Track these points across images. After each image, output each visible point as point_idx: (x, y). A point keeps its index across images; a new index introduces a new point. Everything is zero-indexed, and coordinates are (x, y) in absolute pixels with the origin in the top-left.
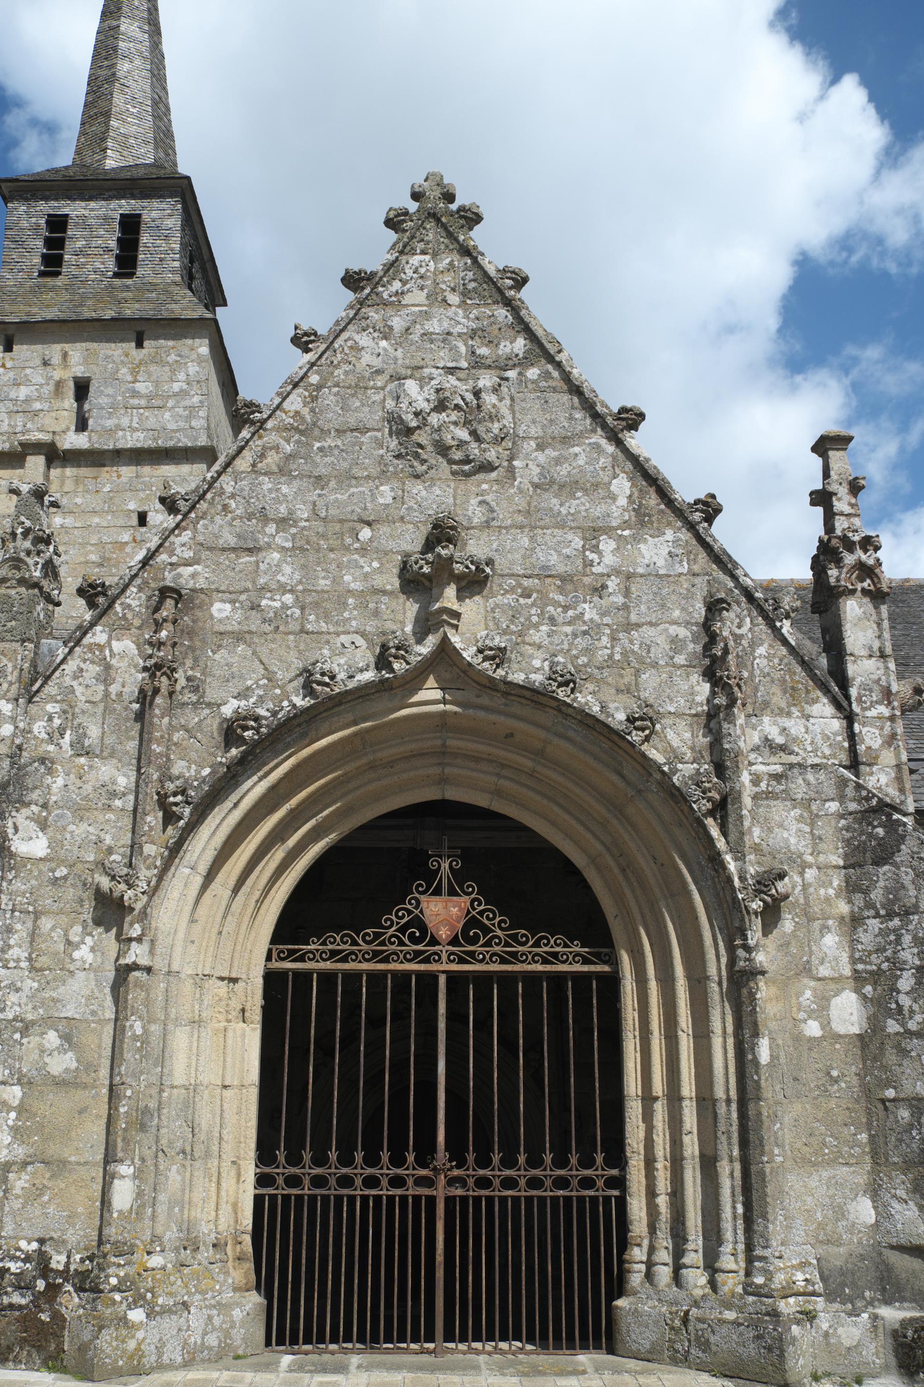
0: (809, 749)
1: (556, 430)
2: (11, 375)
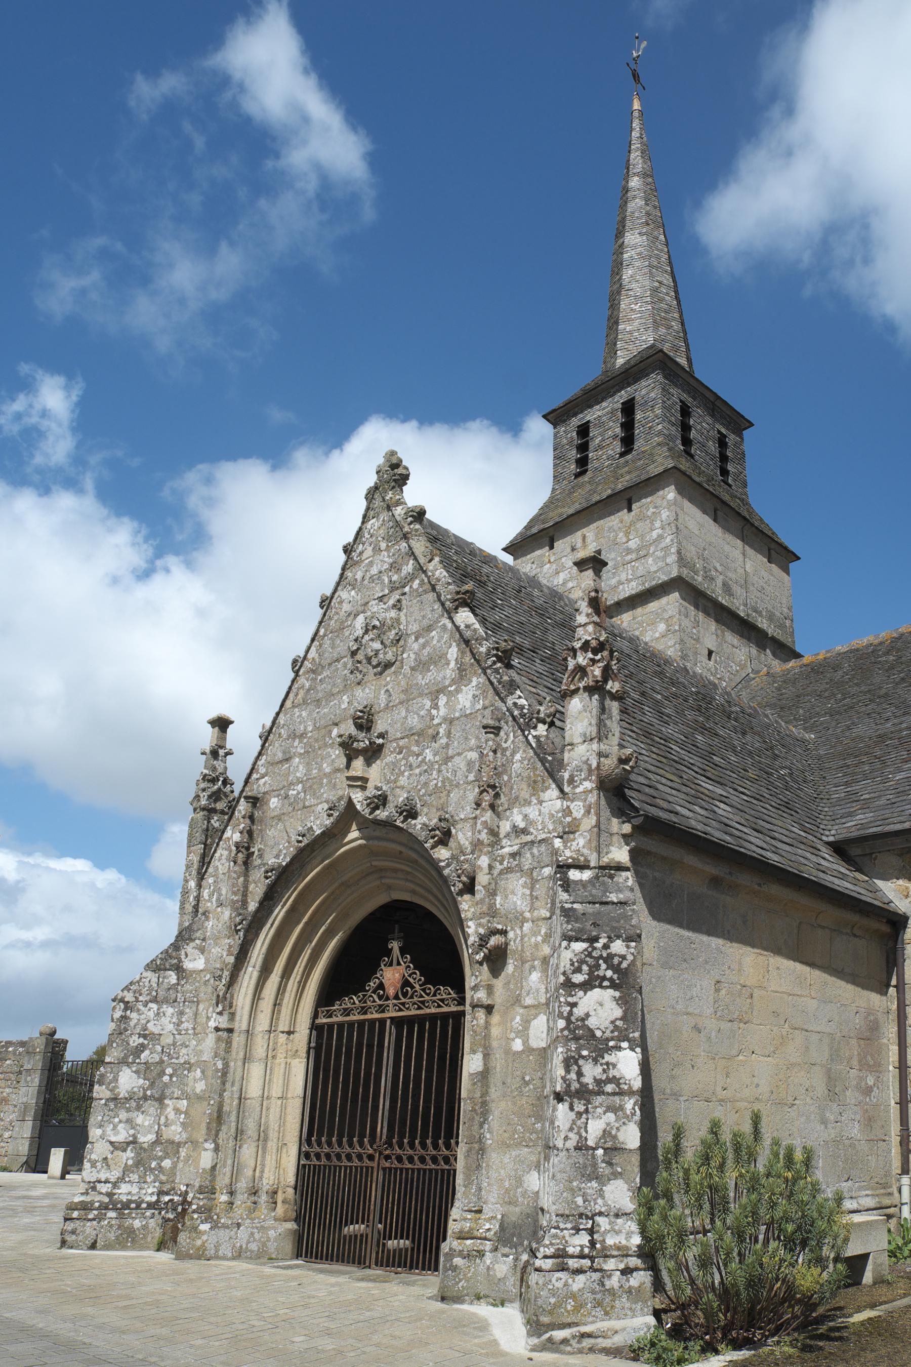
1: (426, 623)
2: (554, 566)
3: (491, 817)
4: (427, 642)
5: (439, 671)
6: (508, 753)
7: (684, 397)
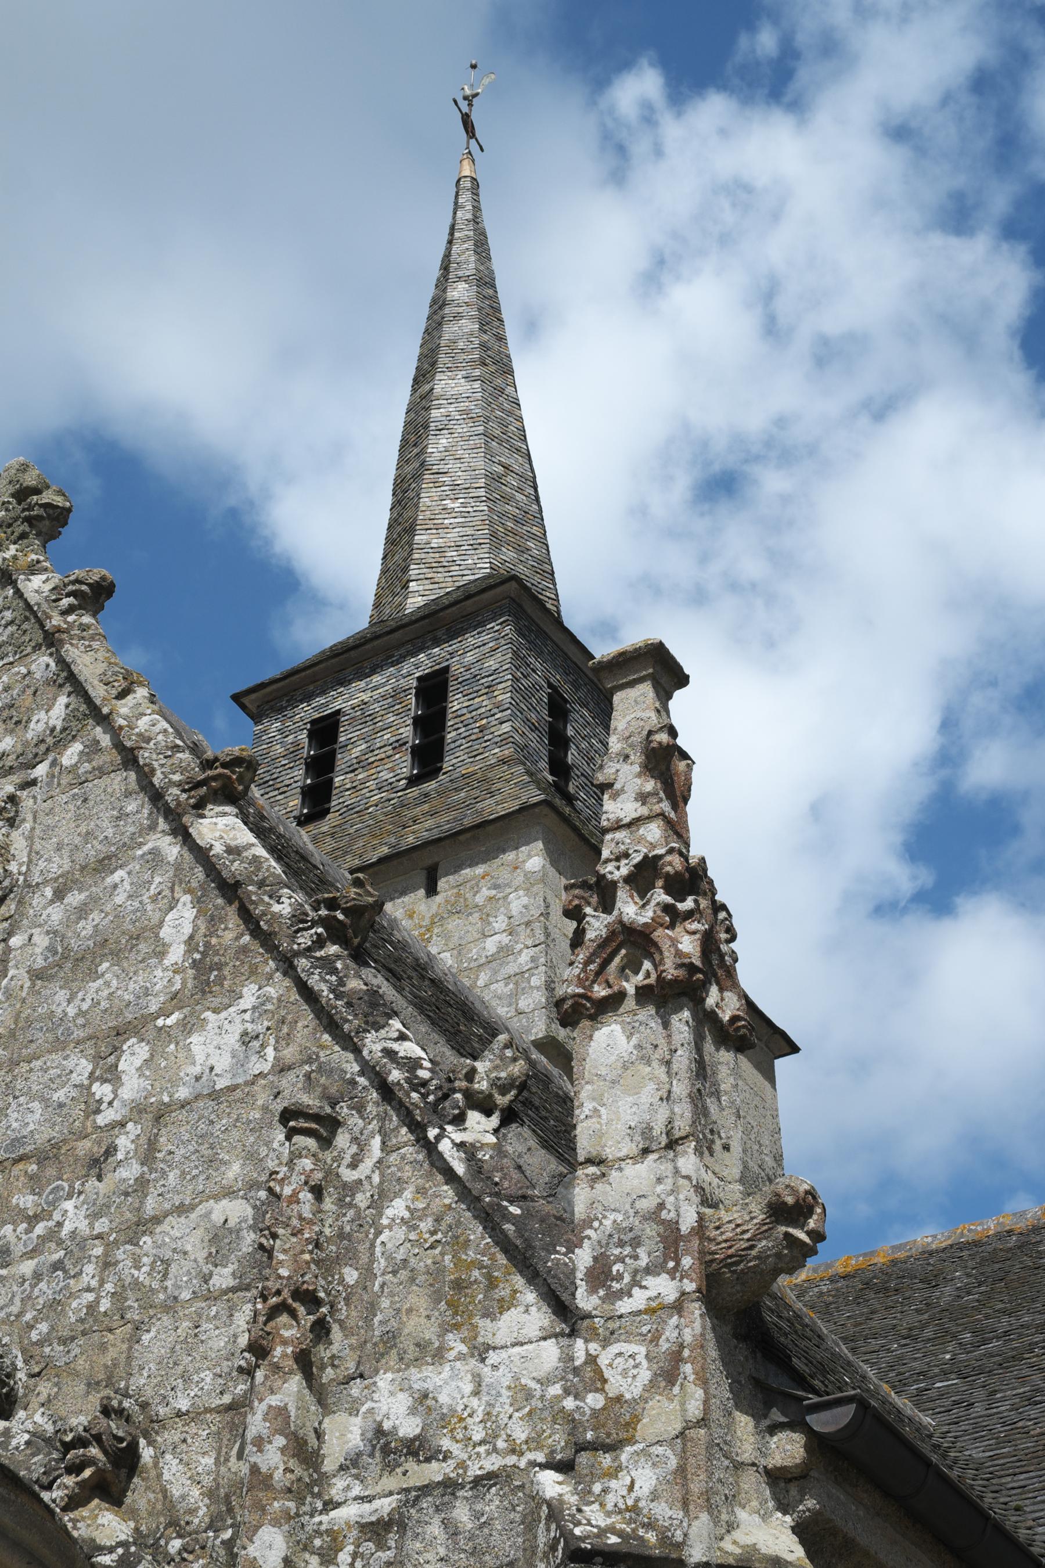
0: (477, 1437)
1: (92, 851)
3: (300, 1397)
4: (95, 900)
5: (126, 976)
6: (361, 1200)
7: (556, 678)
